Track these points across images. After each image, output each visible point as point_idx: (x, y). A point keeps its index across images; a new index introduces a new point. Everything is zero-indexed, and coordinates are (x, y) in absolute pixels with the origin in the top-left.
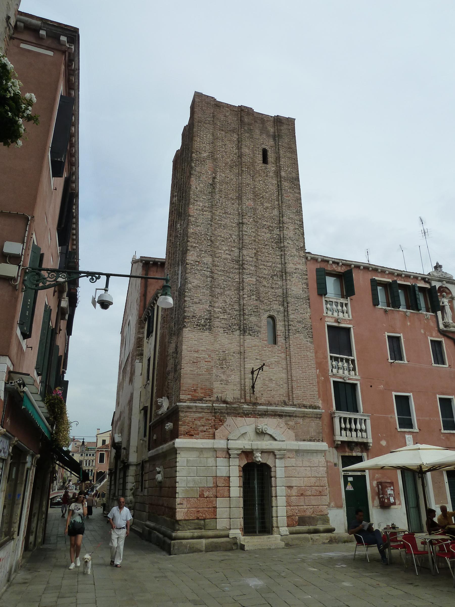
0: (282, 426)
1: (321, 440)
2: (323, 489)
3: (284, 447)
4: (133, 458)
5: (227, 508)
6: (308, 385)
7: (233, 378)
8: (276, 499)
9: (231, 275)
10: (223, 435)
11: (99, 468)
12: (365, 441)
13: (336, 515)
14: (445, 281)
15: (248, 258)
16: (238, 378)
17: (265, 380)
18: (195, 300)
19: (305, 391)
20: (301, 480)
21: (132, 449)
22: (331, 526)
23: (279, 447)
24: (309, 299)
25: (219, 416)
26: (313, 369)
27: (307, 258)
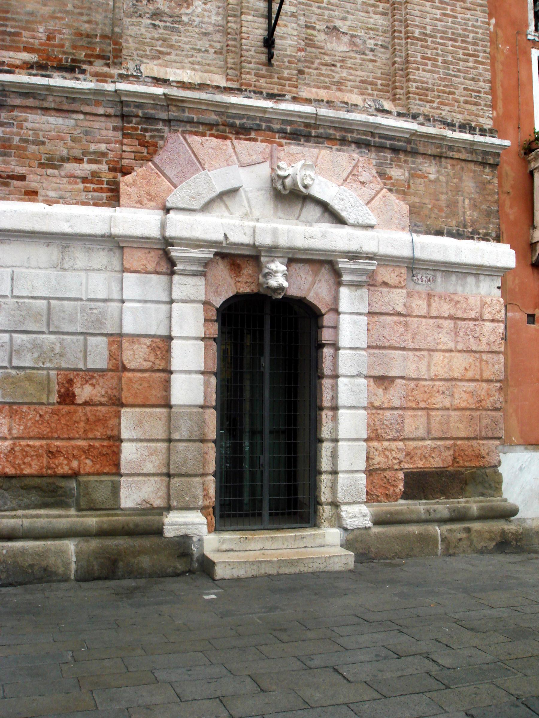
0: (365, 176)
1: (494, 235)
2: (488, 389)
5: (157, 440)
6: (459, 59)
7: (199, 10)
8: (335, 419)
10: (148, 194)
13: (521, 469)
16: (218, 14)
17: (314, 28)
19: (449, 75)
20: (420, 358)
22: (506, 500)
23: (353, 247)
25: (136, 129)
26: (479, 8)
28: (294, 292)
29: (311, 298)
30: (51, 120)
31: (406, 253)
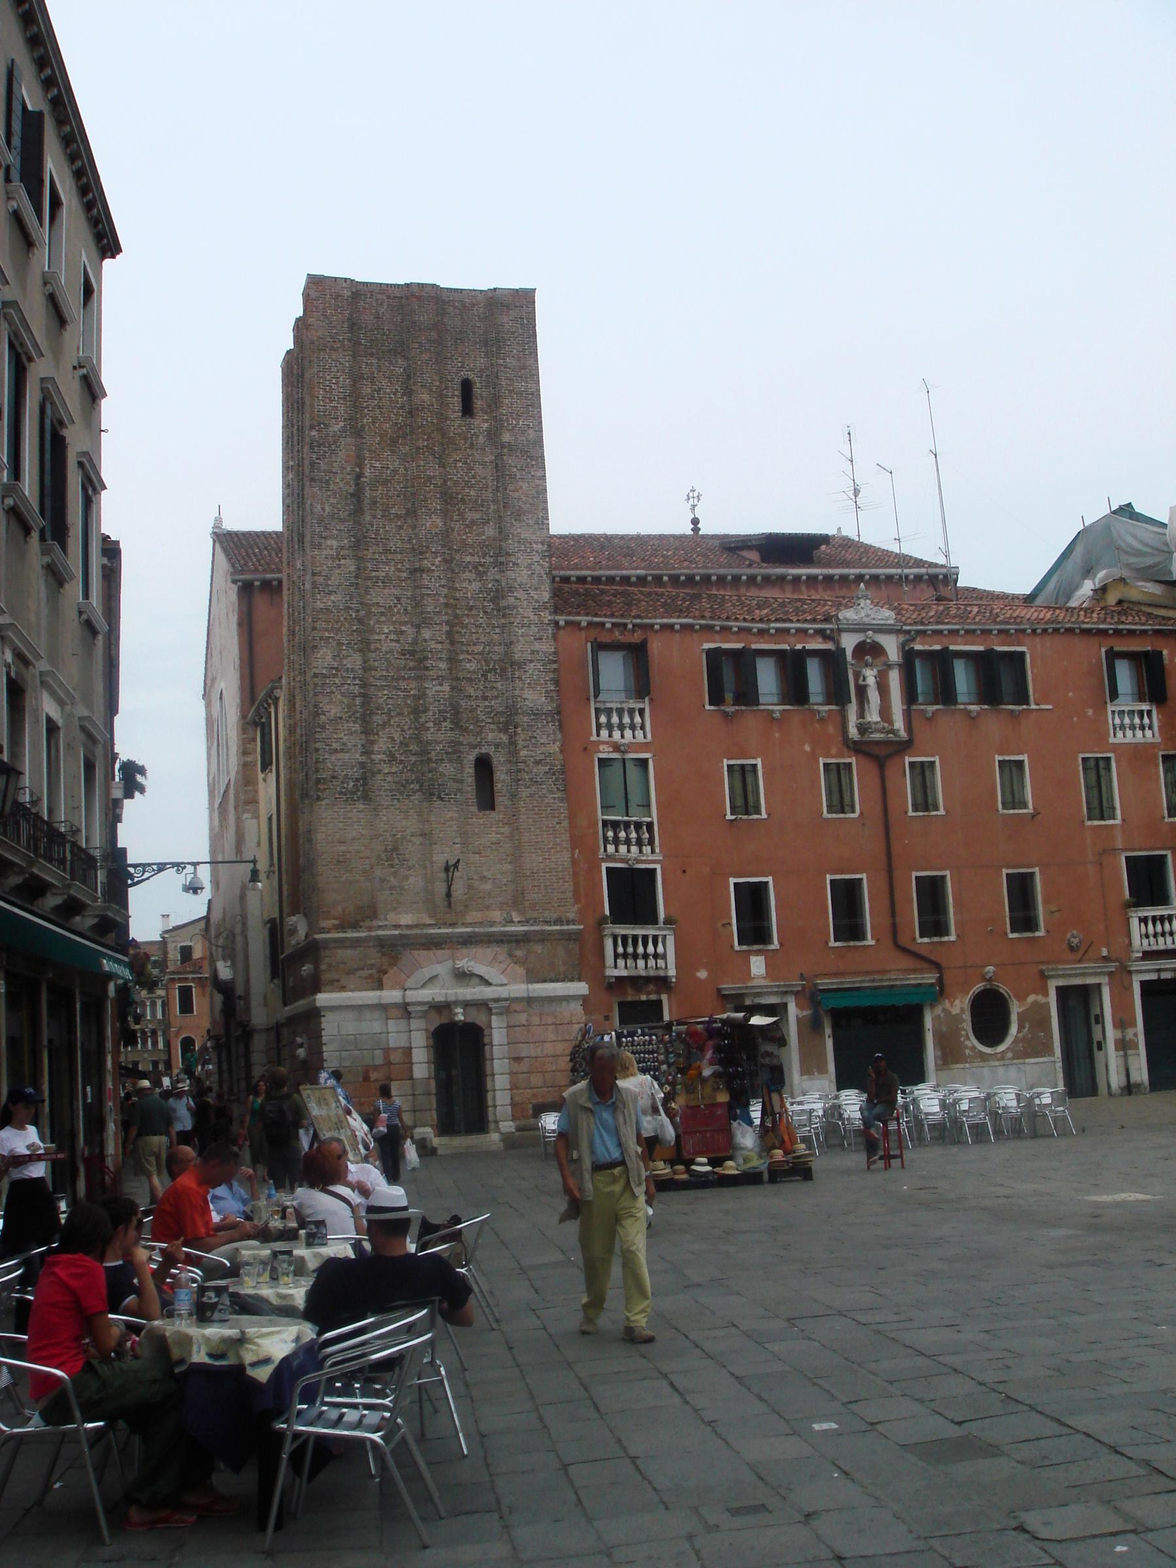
3: (506, 995)
4: (259, 1017)
8: (493, 1080)
9: (403, 684)
11: (181, 1027)
12: (662, 973)
14: (869, 630)
15: (433, 645)
18: (335, 746)
21: (256, 1001)
23: (495, 996)
24: (559, 713)
27: (557, 623)
28: (469, 1020)
29: (478, 1023)
30: (349, 951)
31: (525, 995)
